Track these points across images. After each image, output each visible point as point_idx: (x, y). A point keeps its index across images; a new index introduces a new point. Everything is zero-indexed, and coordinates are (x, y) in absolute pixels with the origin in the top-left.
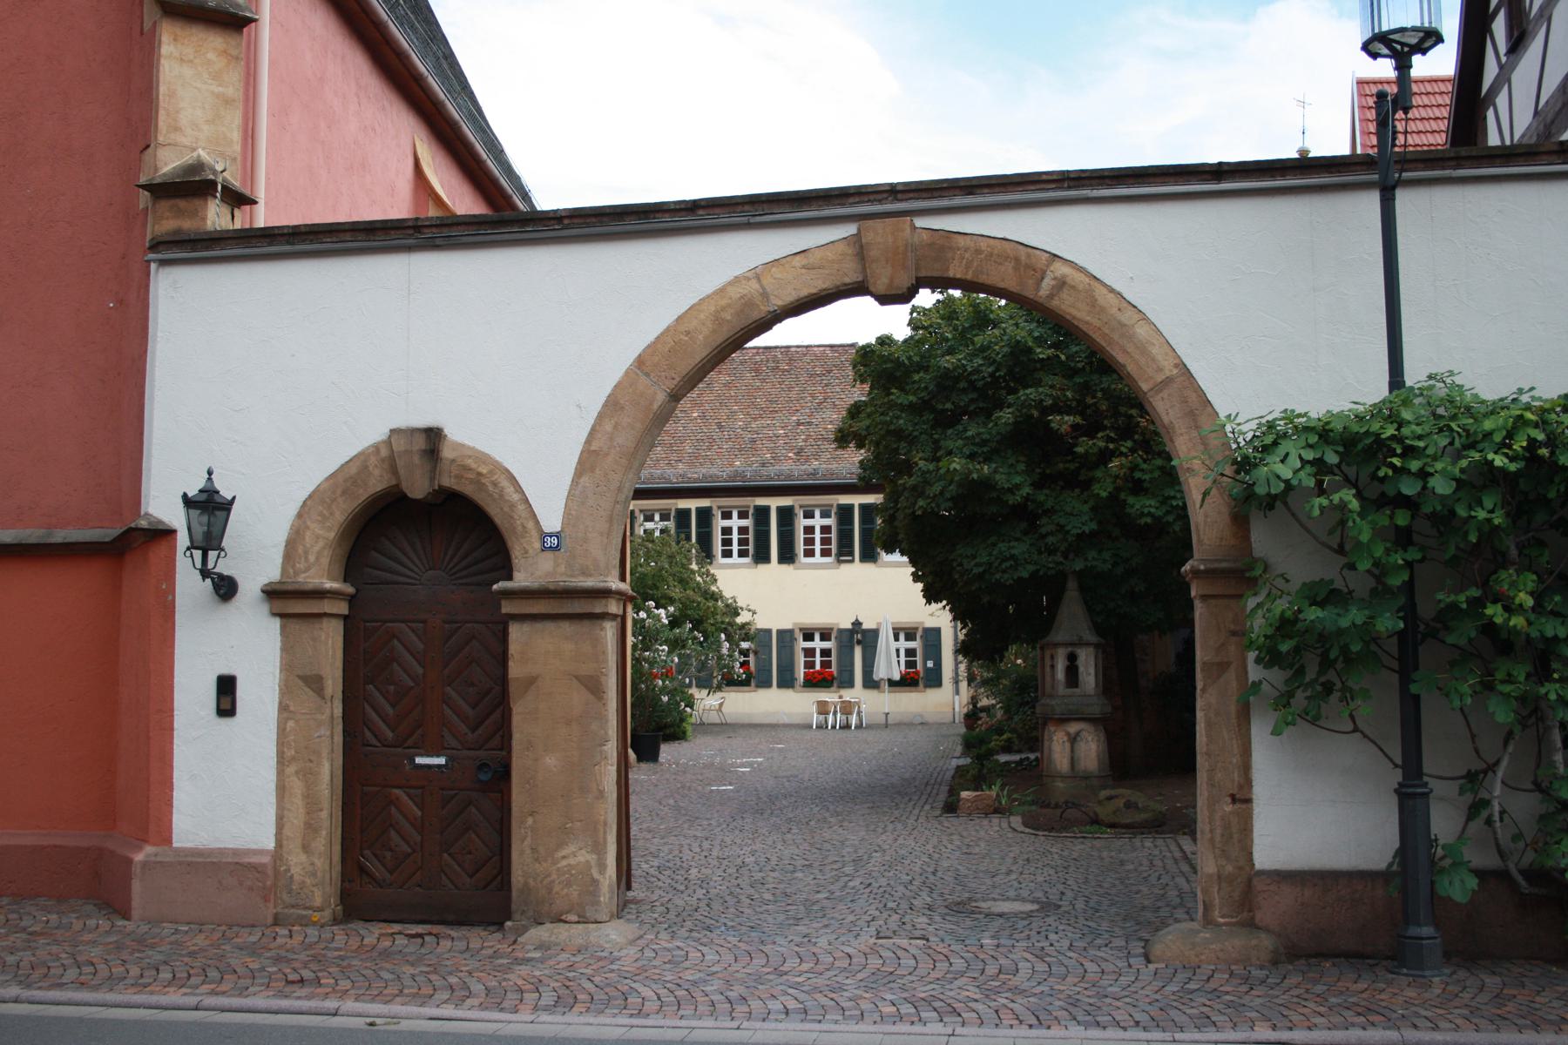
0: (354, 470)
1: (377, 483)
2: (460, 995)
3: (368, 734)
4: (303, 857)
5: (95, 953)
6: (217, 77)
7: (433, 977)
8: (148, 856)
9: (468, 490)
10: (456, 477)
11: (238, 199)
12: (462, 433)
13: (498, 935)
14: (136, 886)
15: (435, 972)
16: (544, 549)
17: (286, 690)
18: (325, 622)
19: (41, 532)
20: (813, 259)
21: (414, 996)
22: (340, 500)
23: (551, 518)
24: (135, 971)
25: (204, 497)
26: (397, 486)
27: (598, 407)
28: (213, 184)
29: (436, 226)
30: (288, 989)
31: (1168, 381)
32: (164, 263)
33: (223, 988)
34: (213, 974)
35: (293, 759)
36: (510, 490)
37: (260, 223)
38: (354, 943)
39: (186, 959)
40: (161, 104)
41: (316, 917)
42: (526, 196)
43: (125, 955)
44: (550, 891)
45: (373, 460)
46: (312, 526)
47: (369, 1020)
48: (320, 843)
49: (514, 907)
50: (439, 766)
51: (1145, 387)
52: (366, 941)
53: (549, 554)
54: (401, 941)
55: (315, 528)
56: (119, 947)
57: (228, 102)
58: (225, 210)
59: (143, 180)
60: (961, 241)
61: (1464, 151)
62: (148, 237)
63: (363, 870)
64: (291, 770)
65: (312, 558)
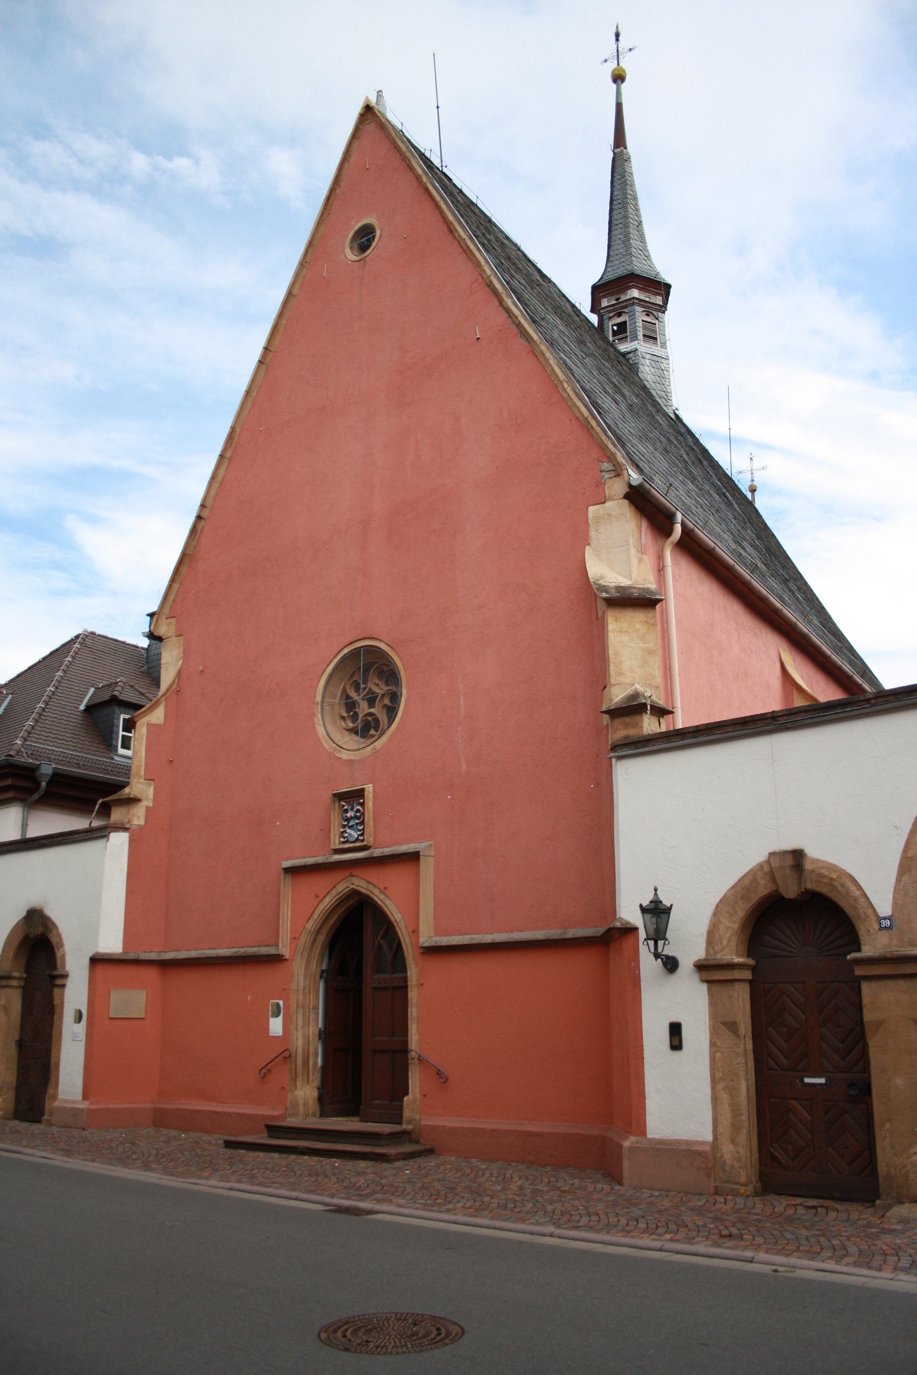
0: (747, 882)
1: (764, 889)
2: (840, 1253)
3: (771, 1062)
4: (732, 1148)
5: (600, 1207)
6: (642, 638)
7: (822, 1239)
8: (633, 1143)
9: (825, 890)
10: (816, 881)
11: (661, 712)
12: (814, 852)
13: (871, 1210)
14: (626, 1164)
15: (823, 1235)
16: (881, 929)
17: (714, 1032)
18: (737, 985)
19: (560, 931)
21: (808, 1252)
22: (740, 902)
23: (884, 907)
24: (623, 1221)
25: (653, 906)
26: (777, 890)
28: (645, 705)
29: (786, 715)
30: (722, 1241)
32: (620, 758)
33: (678, 1237)
34: (673, 1227)
35: (721, 1079)
36: (853, 888)
37: (680, 725)
38: (768, 1210)
39: (656, 1215)
40: (611, 660)
41: (743, 1190)
42: (872, 680)
43: (618, 1210)
45: (760, 874)
46: (724, 921)
47: (774, 1268)
48: (742, 1138)
49: (881, 1190)
50: (821, 1084)
52: (777, 1209)
53: (885, 932)
54: (801, 1210)
55: (726, 922)
56: (615, 1204)
57: (650, 652)
58: (654, 720)
59: (604, 708)
62: (610, 743)
63: (773, 1158)
64: (720, 1086)
65: (725, 942)
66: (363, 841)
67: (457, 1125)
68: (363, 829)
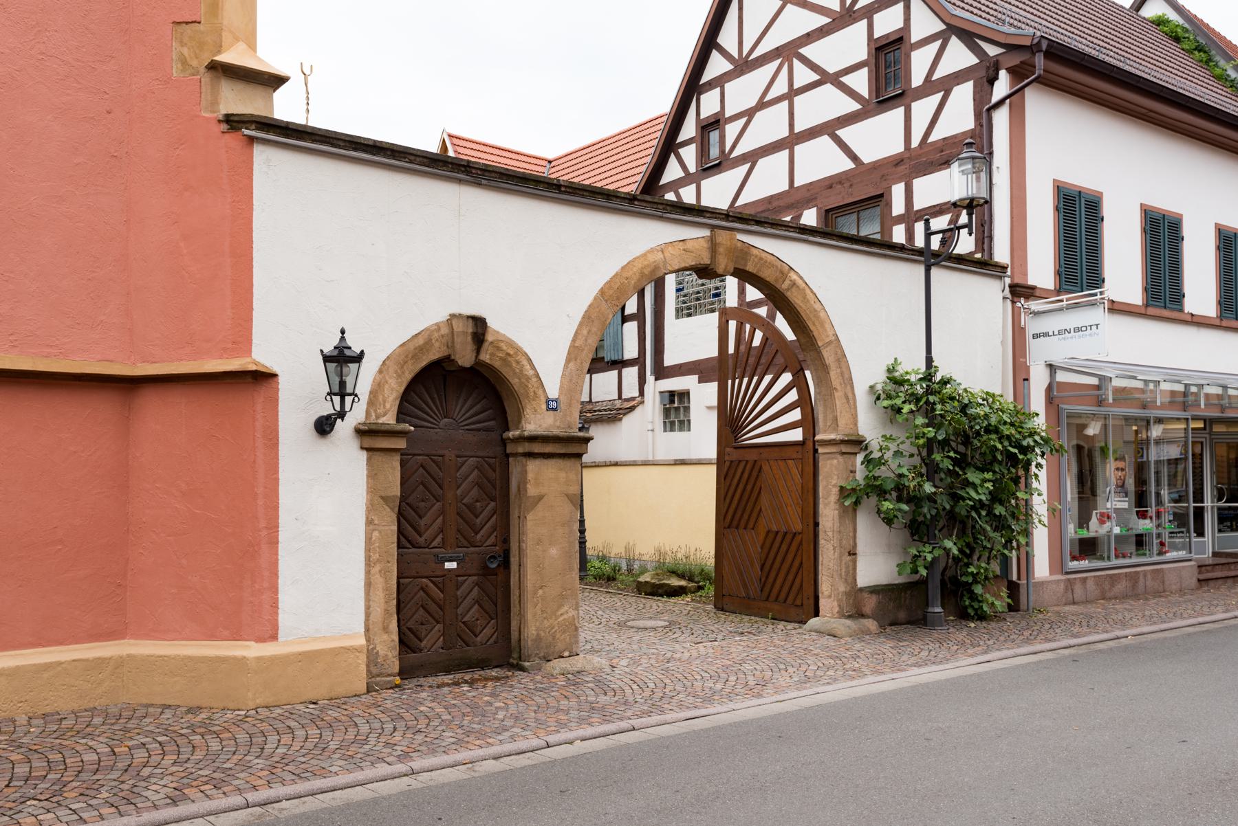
0: (421, 341)
1: (434, 355)
4: (385, 637)
16: (548, 409)
20: (689, 245)
23: (553, 391)
25: (335, 353)
27: (579, 318)
31: (830, 343)
44: (554, 638)
51: (820, 344)
53: (551, 413)
60: (755, 252)
61: (648, 198)
64: (377, 568)
65: (388, 406)
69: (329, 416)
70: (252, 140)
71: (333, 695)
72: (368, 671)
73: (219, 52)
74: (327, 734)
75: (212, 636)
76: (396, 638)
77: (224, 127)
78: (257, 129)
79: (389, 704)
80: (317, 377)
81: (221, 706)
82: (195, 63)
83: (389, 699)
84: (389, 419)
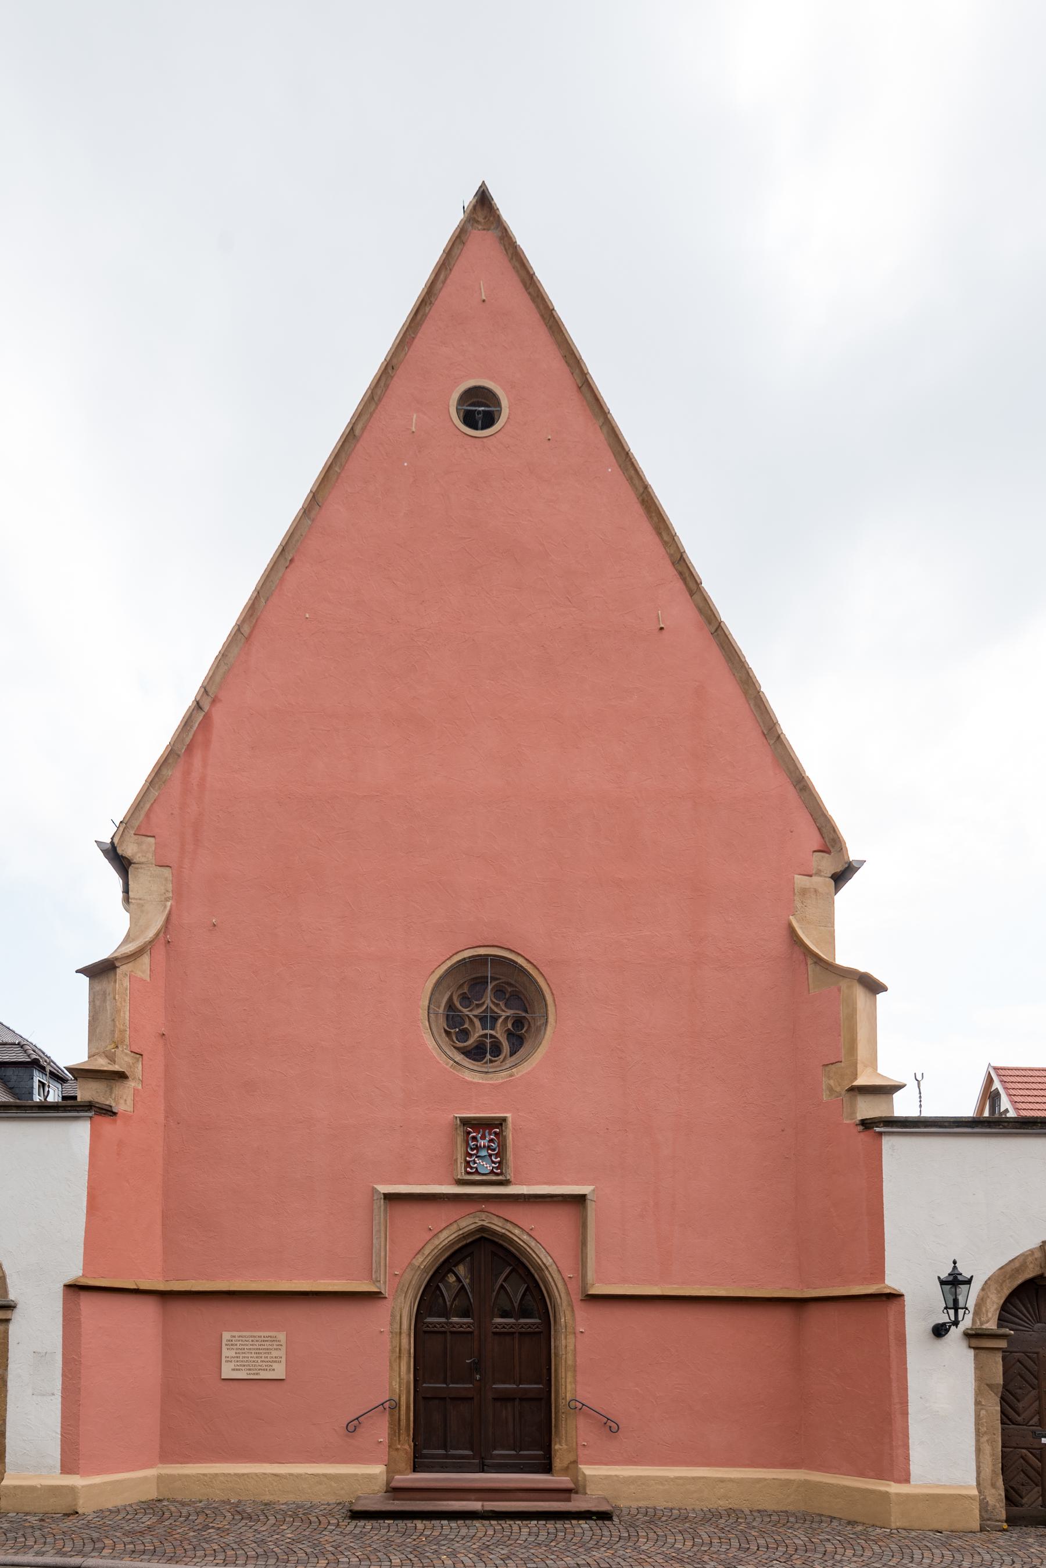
0: (1017, 1264)
4: (993, 1491)
25: (951, 1278)
35: (985, 1433)
64: (985, 1438)
65: (990, 1315)
66: (501, 1174)
67: (787, 1477)
68: (499, 1162)
69: (944, 1324)
70: (881, 1134)
71: (953, 1528)
72: (980, 1515)
73: (856, 1079)
74: (958, 1556)
75: (862, 1474)
76: (1003, 1494)
77: (861, 1128)
78: (885, 1126)
79: (1001, 1542)
80: (936, 1297)
81: (871, 1523)
82: (838, 1089)
83: (1002, 1539)
84: (991, 1325)
